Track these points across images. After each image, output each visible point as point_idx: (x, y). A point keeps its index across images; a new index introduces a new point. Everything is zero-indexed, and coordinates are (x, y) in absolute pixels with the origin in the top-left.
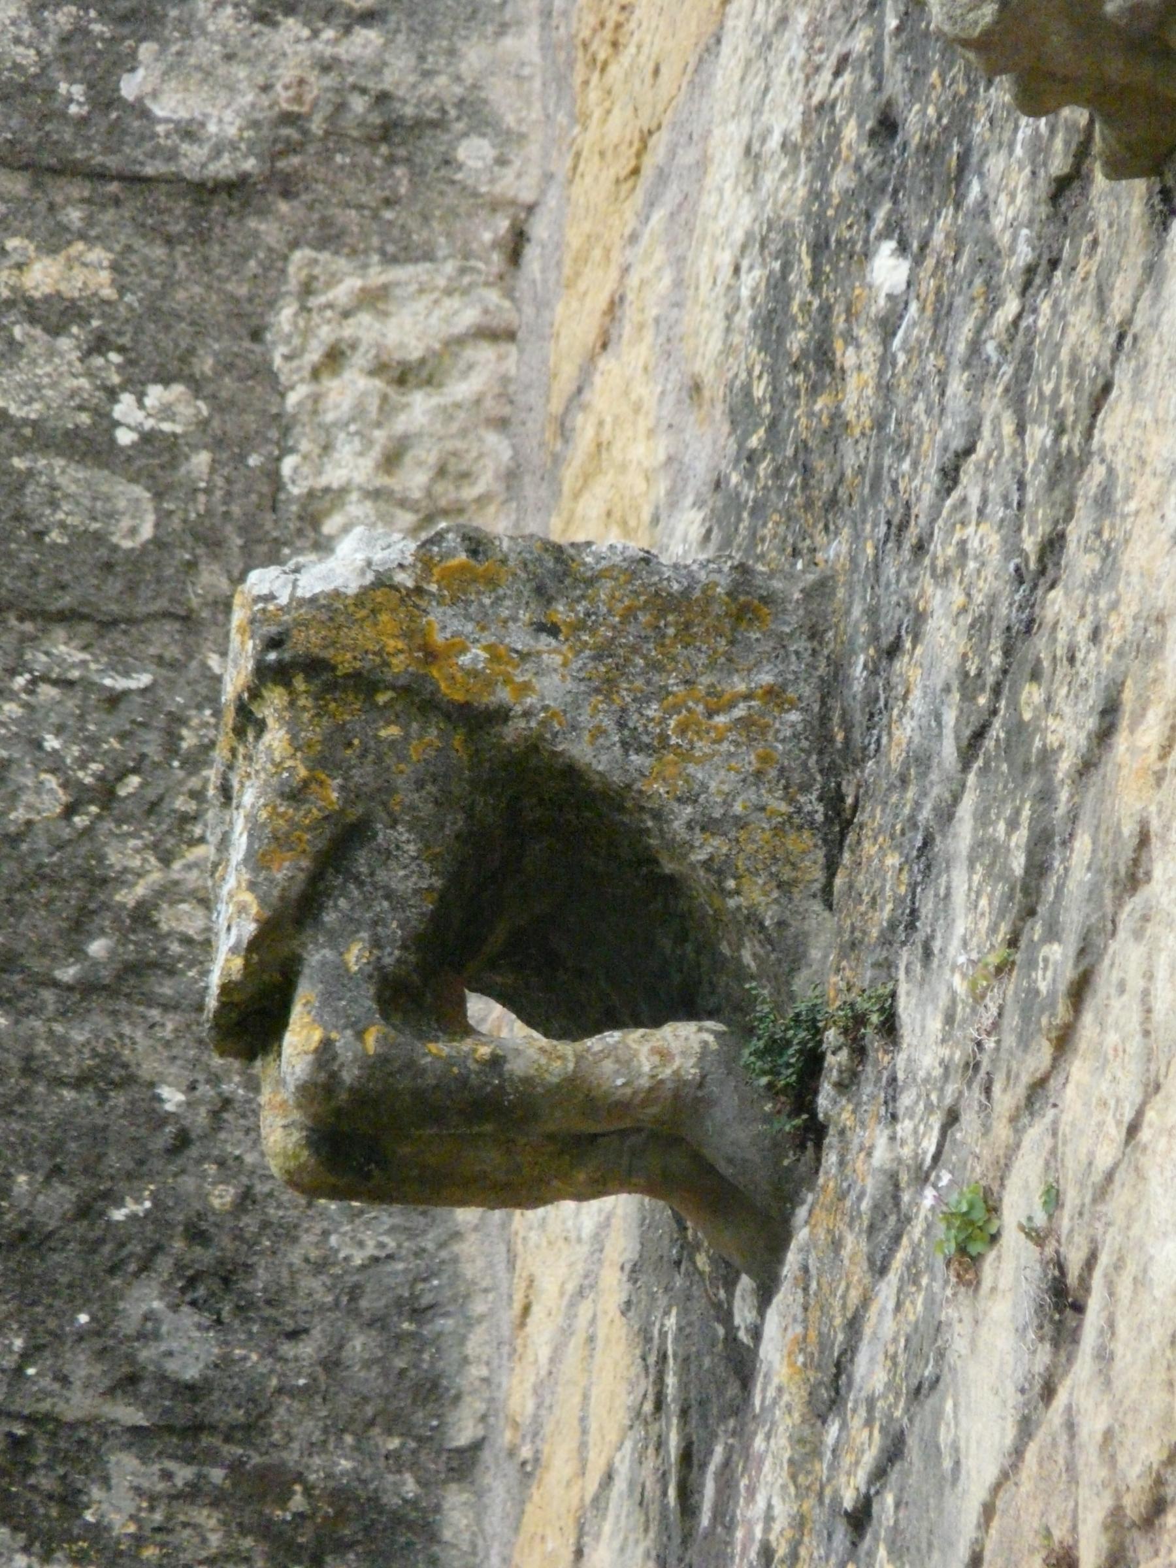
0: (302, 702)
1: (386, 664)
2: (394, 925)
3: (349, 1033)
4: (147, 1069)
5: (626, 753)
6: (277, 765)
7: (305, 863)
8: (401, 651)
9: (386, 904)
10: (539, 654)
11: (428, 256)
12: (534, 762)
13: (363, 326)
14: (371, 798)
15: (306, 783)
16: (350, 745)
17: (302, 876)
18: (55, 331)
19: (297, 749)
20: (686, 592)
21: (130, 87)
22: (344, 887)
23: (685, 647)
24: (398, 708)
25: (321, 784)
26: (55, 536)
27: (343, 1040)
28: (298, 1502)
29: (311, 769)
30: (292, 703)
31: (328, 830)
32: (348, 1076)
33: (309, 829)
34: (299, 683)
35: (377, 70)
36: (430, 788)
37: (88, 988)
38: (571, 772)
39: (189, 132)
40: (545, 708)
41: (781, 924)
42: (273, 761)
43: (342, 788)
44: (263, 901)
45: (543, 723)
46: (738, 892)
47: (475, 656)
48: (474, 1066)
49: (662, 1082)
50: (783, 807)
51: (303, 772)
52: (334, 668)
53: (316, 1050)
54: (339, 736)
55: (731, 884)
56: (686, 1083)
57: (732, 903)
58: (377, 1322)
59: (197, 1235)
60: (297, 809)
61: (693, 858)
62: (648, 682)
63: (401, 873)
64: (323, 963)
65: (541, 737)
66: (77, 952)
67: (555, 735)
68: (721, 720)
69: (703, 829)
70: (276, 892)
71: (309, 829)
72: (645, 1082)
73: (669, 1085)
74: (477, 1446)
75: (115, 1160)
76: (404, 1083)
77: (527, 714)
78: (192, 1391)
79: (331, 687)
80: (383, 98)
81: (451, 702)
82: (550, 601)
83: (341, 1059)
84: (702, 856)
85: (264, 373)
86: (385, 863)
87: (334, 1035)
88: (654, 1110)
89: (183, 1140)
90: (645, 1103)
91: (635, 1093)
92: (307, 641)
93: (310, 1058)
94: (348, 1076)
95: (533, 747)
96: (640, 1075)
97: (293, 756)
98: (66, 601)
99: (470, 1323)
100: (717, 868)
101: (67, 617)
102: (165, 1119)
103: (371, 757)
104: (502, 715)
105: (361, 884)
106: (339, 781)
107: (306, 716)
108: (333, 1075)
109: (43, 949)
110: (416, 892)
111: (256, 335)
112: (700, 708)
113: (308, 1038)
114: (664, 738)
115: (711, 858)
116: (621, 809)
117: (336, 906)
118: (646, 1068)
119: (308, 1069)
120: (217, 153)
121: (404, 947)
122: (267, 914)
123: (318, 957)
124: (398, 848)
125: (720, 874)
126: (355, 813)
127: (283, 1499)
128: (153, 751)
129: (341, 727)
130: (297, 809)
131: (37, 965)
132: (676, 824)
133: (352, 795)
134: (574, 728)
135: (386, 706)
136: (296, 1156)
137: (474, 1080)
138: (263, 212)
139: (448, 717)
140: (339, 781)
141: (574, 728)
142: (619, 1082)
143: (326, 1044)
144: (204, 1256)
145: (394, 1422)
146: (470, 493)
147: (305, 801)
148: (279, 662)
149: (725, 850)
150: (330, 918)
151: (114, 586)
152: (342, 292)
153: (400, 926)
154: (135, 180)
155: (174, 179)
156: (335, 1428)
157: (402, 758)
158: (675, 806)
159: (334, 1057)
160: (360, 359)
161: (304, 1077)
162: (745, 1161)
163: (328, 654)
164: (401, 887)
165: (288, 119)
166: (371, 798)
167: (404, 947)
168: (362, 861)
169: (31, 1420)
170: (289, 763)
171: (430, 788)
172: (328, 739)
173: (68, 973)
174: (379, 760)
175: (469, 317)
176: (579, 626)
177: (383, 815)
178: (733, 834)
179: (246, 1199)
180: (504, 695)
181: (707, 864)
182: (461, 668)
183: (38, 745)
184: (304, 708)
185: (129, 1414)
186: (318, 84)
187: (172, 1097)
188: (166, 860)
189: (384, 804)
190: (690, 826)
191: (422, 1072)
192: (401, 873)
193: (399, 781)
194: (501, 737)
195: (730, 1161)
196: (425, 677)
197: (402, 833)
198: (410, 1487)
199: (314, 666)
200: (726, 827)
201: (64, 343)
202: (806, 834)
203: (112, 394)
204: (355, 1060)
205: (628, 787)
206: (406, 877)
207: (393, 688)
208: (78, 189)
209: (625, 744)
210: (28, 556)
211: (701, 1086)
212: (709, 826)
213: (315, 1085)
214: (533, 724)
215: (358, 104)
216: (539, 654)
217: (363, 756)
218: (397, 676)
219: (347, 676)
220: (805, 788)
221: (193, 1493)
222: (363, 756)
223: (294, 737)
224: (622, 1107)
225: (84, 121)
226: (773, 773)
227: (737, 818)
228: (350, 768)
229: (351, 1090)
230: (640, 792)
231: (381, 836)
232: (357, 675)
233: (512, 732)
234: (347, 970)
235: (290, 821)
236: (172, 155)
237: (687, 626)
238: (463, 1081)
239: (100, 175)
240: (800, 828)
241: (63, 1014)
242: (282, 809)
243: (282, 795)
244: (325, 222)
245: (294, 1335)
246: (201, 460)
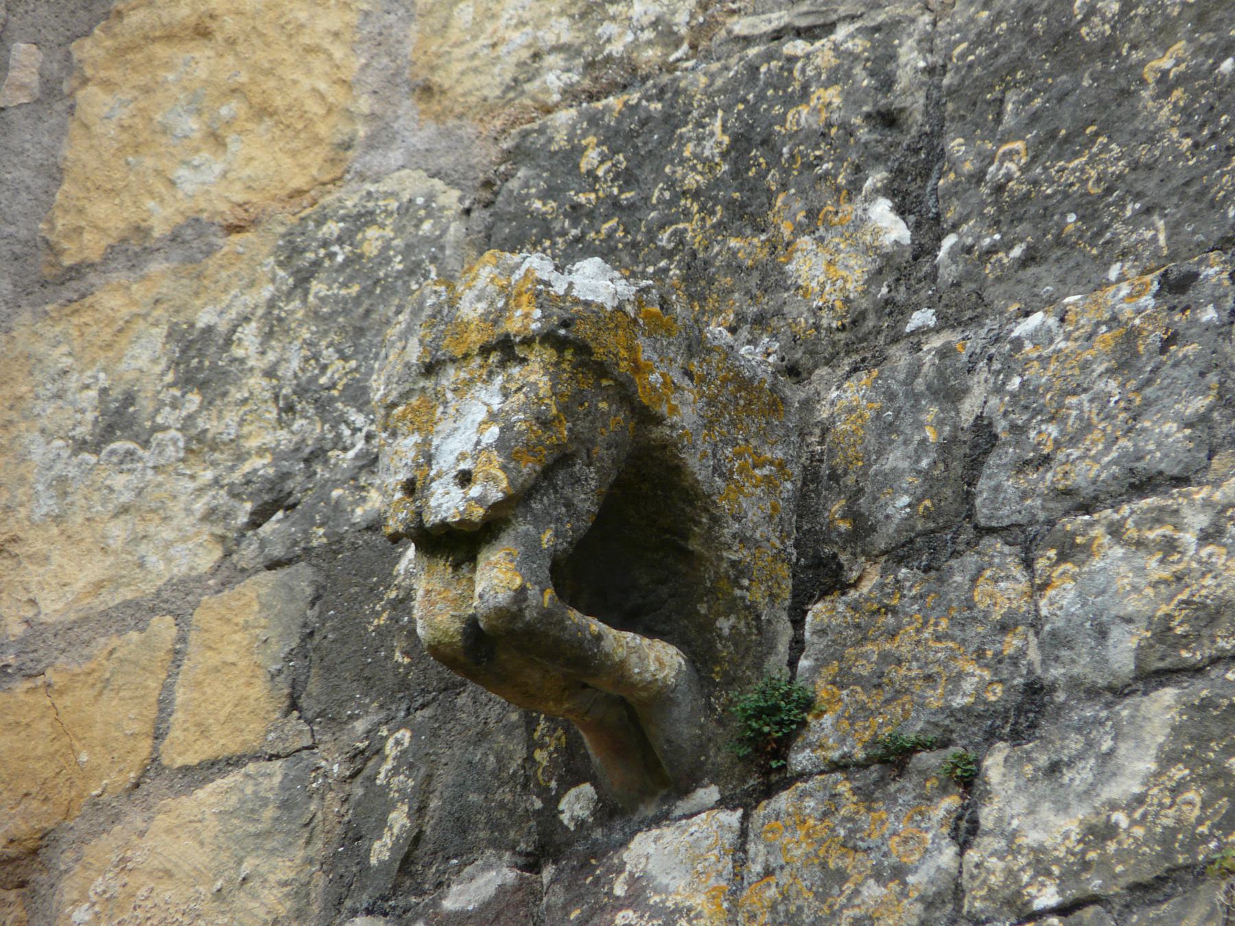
0: (564, 366)
1: (617, 364)
2: (568, 526)
3: (537, 587)
5: (713, 473)
6: (540, 399)
7: (538, 468)
8: (625, 359)
9: (564, 510)
10: (683, 390)
12: (657, 454)
14: (582, 443)
15: (556, 417)
16: (582, 404)
17: (534, 475)
19: (554, 394)
20: (751, 379)
22: (547, 491)
23: (748, 416)
24: (611, 392)
25: (560, 422)
27: (533, 591)
29: (559, 411)
30: (557, 364)
31: (556, 454)
32: (529, 615)
33: (547, 448)
34: (568, 355)
36: (613, 451)
38: (678, 469)
40: (683, 428)
41: (769, 621)
42: (537, 395)
44: (511, 482)
45: (679, 436)
46: (748, 589)
47: (655, 378)
48: (589, 637)
49: (657, 680)
50: (778, 544)
51: (554, 411)
52: (591, 354)
53: (516, 590)
54: (578, 397)
55: (746, 582)
56: (667, 686)
57: (738, 592)
60: (544, 432)
61: (725, 554)
62: (729, 432)
63: (583, 496)
64: (526, 534)
65: (675, 445)
67: (684, 447)
68: (757, 472)
69: (741, 541)
70: (520, 480)
71: (547, 448)
72: (648, 676)
73: (660, 684)
76: (553, 632)
77: (672, 427)
79: (583, 364)
81: (640, 402)
82: (691, 356)
83: (528, 603)
84: (734, 557)
86: (573, 484)
87: (528, 585)
88: (644, 694)
90: (645, 688)
91: (641, 681)
92: (584, 331)
93: (512, 593)
94: (529, 615)
96: (647, 671)
97: (550, 398)
103: (590, 418)
104: (659, 420)
105: (556, 492)
106: (570, 425)
107: (566, 376)
108: (521, 610)
113: (512, 580)
114: (731, 472)
115: (740, 562)
117: (541, 500)
118: (652, 669)
119: (508, 600)
121: (570, 543)
122: (512, 492)
123: (523, 528)
124: (586, 480)
126: (573, 447)
129: (581, 391)
130: (544, 432)
132: (726, 531)
133: (574, 436)
134: (694, 447)
136: (452, 636)
137: (586, 644)
139: (633, 410)
140: (570, 425)
141: (694, 447)
142: (637, 670)
143: (522, 590)
147: (550, 429)
148: (566, 337)
149: (748, 559)
150: (536, 506)
153: (572, 529)
157: (605, 426)
158: (730, 521)
159: (525, 599)
161: (504, 604)
163: (593, 345)
164: (580, 505)
166: (582, 443)
167: (570, 543)
168: (561, 477)
170: (547, 401)
171: (613, 451)
172: (572, 397)
174: (593, 422)
176: (702, 380)
178: (753, 550)
180: (664, 409)
181: (734, 564)
182: (650, 383)
184: (564, 371)
189: (588, 450)
190: (734, 536)
191: (565, 628)
192: (583, 496)
193: (600, 439)
194: (650, 432)
195: (669, 741)
196: (632, 381)
197: (592, 473)
199: (582, 349)
200: (751, 545)
202: (786, 566)
205: (709, 496)
206: (585, 500)
207: (615, 380)
209: (715, 469)
211: (673, 692)
212: (744, 540)
213: (508, 611)
214: (674, 435)
216: (683, 390)
217: (586, 415)
218: (621, 374)
219: (596, 362)
220: (788, 536)
222: (586, 415)
223: (553, 387)
226: (777, 520)
227: (756, 541)
228: (578, 419)
229: (528, 624)
230: (714, 502)
231: (578, 467)
232: (601, 364)
233: (657, 433)
234: (540, 545)
235: (538, 437)
237: (750, 403)
238: (581, 642)
240: (783, 561)
242: (535, 428)
243: (537, 419)
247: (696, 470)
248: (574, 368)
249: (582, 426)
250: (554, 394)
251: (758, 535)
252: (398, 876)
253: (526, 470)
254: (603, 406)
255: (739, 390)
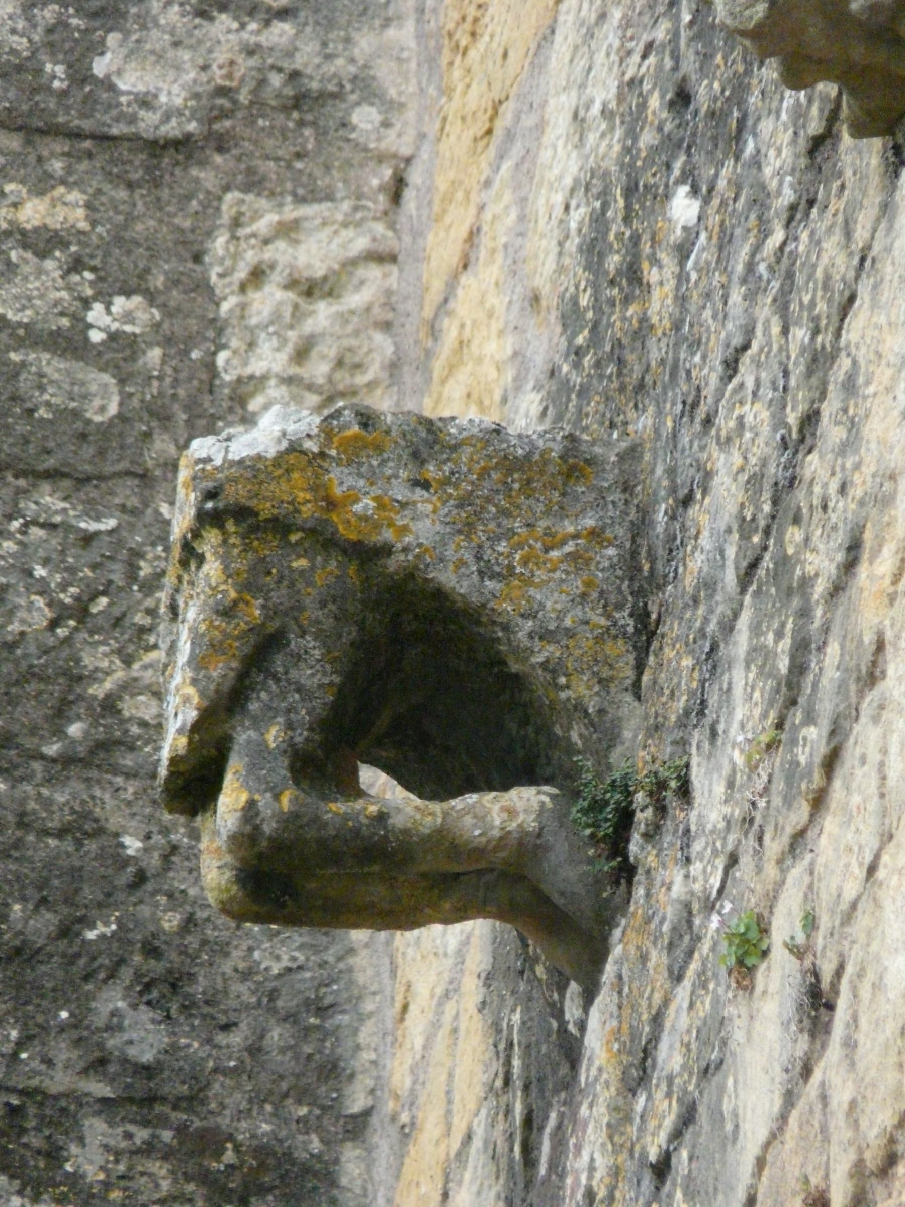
0: (232, 540)
1: (297, 511)
2: (303, 712)
3: (268, 795)
4: (113, 823)
5: (482, 580)
6: (213, 589)
7: (235, 664)
8: (309, 501)
9: (297, 696)
10: (415, 503)
11: (330, 197)
12: (411, 586)
13: (280, 251)
14: (286, 614)
15: (235, 603)
16: (269, 573)
17: (232, 674)
18: (43, 255)
19: (229, 577)
20: (528, 456)
21: (100, 67)
23: (527, 498)
24: (307, 545)
25: (247, 603)
26: (42, 413)
27: (264, 801)
28: (229, 1156)
29: (239, 592)
30: (225, 541)
31: (253, 639)
32: (268, 828)
33: (238, 638)
34: (230, 526)
35: (290, 54)
36: (331, 606)
37: (67, 761)
38: (440, 595)
39: (145, 101)
40: (420, 545)
41: (601, 711)
42: (210, 586)
43: (263, 607)
44: (202, 694)
45: (418, 557)
46: (568, 687)
47: (365, 505)
48: (365, 821)
49: (509, 833)
50: (603, 621)
51: (233, 594)
52: (257, 514)
53: (243, 809)
54: (261, 567)
55: (563, 680)
56: (528, 834)
57: (563, 695)
58: (290, 1018)
59: (151, 951)
60: (228, 623)
61: (533, 660)
62: (499, 525)
63: (309, 672)
64: (249, 742)
65: (416, 567)
66: (59, 733)
67: (427, 566)
68: (555, 554)
69: (541, 638)
70: (212, 687)
71: (238, 638)
72: (496, 833)
73: (515, 835)
74: (367, 1113)
75: (89, 893)
76: (311, 834)
77: (405, 550)
78: (148, 1071)
79: (255, 529)
80: (295, 75)
81: (347, 540)
82: (423, 462)
83: (262, 815)
84: (540, 659)
85: (203, 287)
86: (296, 665)
87: (257, 797)
88: (503, 854)
89: (141, 878)
90: (496, 849)
91: (488, 842)
92: (236, 494)
93: (239, 814)
94: (268, 828)
95: (410, 575)
96: (492, 828)
97: (225, 582)
98: (50, 462)
99: (362, 1018)
100: (551, 668)
101: (52, 475)
102: (127, 861)
103: (285, 583)
104: (386, 550)
105: (277, 680)
106: (261, 601)
107: (236, 551)
108: (257, 828)
109: (33, 731)
110: (320, 686)
111: (197, 258)
112: (539, 545)
113: (237, 799)
114: (511, 568)
115: (547, 661)
116: (478, 623)
117: (258, 697)
118: (497, 822)
120: (167, 118)
121: (311, 729)
122: (206, 703)
123: (244, 737)
124: (306, 652)
125: (554, 672)
126: (273, 626)
127: (218, 1154)
128: (118, 579)
129: (263, 560)
130: (228, 623)
131: (29, 743)
132: (520, 634)
133: (271, 612)
134: (442, 560)
135: (297, 543)
136: (228, 890)
137: (365, 832)
138: (202, 164)
139: (345, 552)
140: (261, 601)
141: (442, 560)
142: (477, 833)
143: (251, 804)
144: (157, 967)
145: (303, 1095)
146: (361, 379)
147: (234, 617)
148: (215, 509)
149: (558, 654)
150: (254, 706)
151: (88, 451)
152: (264, 225)
153: (308, 713)
154: (104, 139)
155: (134, 137)
156: (258, 1099)
157: (310, 584)
158: (520, 620)
159: (257, 814)
160: (277, 277)
161: (234, 829)
162: (573, 893)
163: (252, 503)
164: (309, 683)
165: (222, 91)
166: (286, 614)
167: (311, 729)
169: (24, 1093)
170: (222, 587)
171: (331, 606)
172: (252, 569)
173: (52, 749)
174: (292, 585)
175: (361, 244)
176: (446, 482)
177: (295, 627)
178: (564, 642)
179: (189, 923)
180: (388, 535)
181: (544, 665)
182: (355, 514)
183: (29, 573)
184: (234, 545)
185: (99, 1089)
186: (245, 65)
187: (133, 845)
188: (128, 662)
189: (296, 619)
190: (531, 636)
191: (325, 825)
192: (309, 672)
193: (307, 601)
195: (562, 894)
196: (327, 521)
197: (309, 641)
198: (316, 1145)
199: (241, 513)
200: (559, 637)
201: (49, 264)
202: (620, 642)
203: (86, 303)
204: (273, 816)
205: (484, 606)
206: (313, 675)
207: (303, 529)
208: (60, 146)
209: (481, 573)
210: (21, 428)
211: (539, 836)
212: (546, 636)
213: (243, 835)
214: (410, 557)
215: (276, 80)
216: (415, 503)
217: (279, 582)
218: (305, 521)
219: (267, 520)
220: (619, 607)
221: (148, 1149)
222: (279, 582)
223: (226, 568)
224: (479, 852)
225: (64, 93)
226: (595, 595)
227: (567, 630)
228: (270, 591)
229: (270, 839)
230: (493, 610)
231: (293, 644)
232: (275, 520)
233: (394, 563)
234: (267, 747)
235: (223, 632)
236: (133, 119)
237: (529, 482)
238: (356, 832)
239: (77, 135)
240: (616, 637)
241: (48, 781)
242: (217, 623)
243: (217, 612)
244: (250, 171)
245: (226, 1028)
246: (155, 354)
247: (452, 584)
248: (243, 538)
249: (279, 596)
250: (229, 577)
251: (568, 622)
252: (525, 1171)
253: (215, 674)
254: (301, 563)
255: (510, 471)
